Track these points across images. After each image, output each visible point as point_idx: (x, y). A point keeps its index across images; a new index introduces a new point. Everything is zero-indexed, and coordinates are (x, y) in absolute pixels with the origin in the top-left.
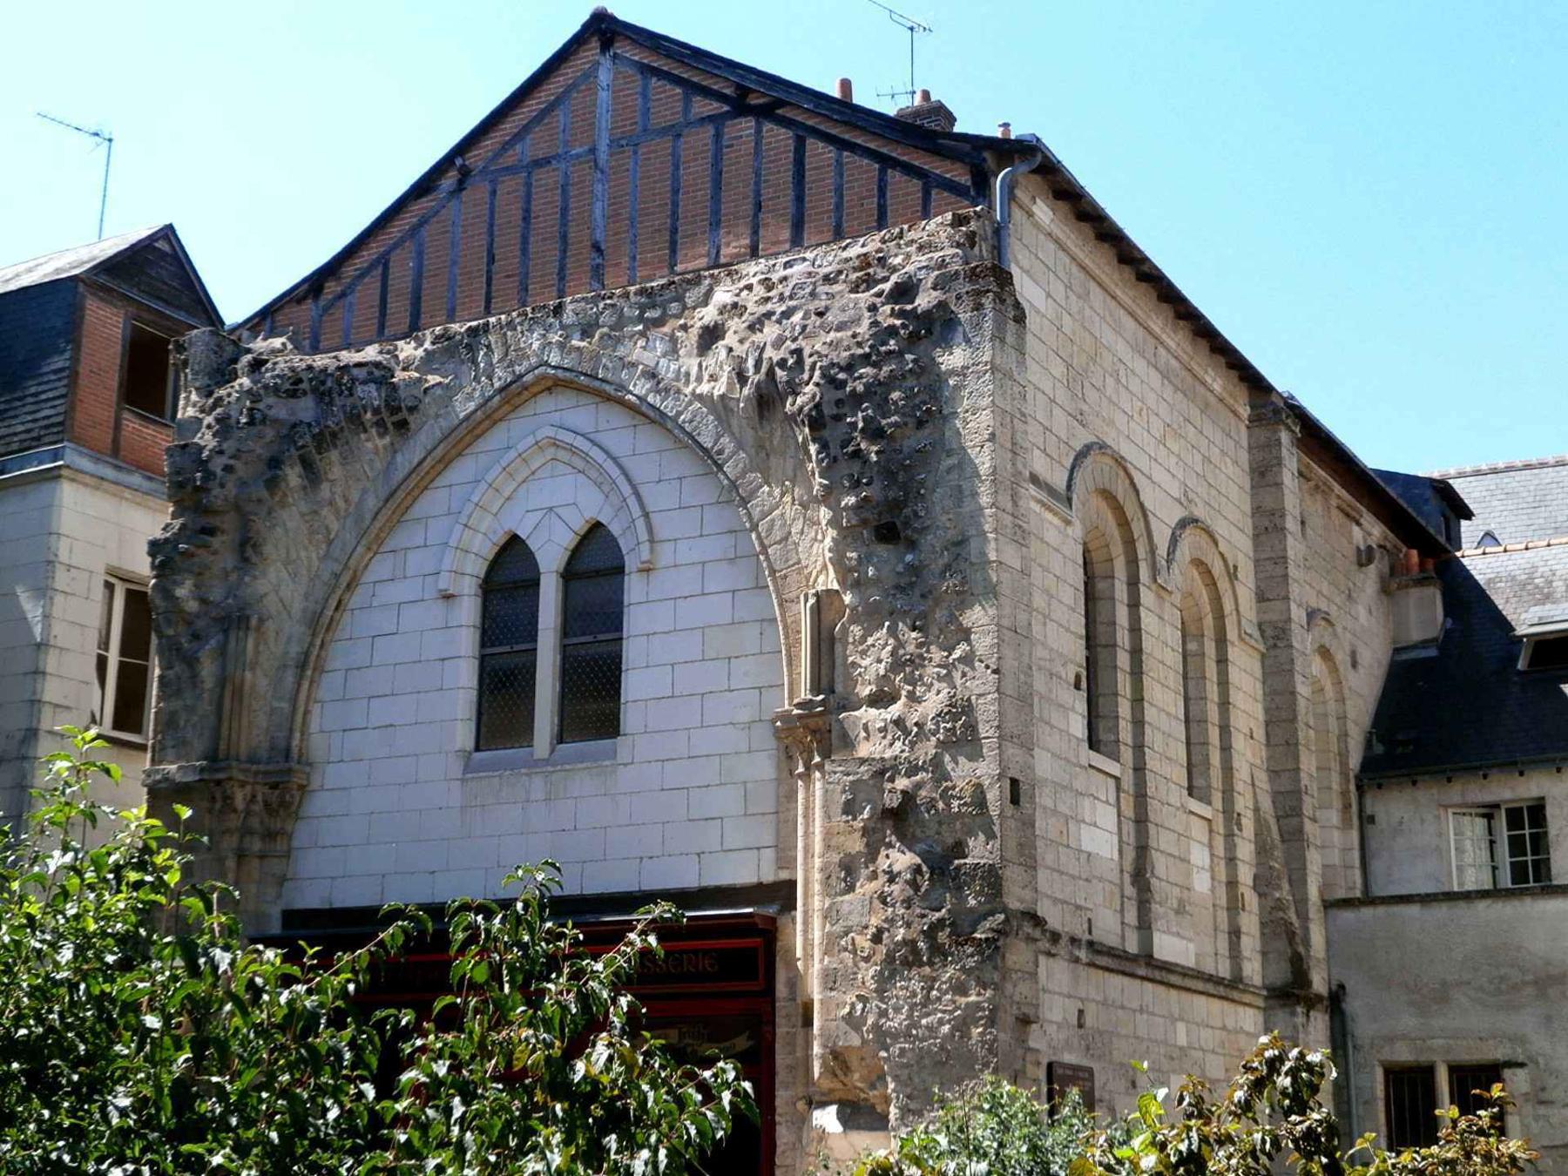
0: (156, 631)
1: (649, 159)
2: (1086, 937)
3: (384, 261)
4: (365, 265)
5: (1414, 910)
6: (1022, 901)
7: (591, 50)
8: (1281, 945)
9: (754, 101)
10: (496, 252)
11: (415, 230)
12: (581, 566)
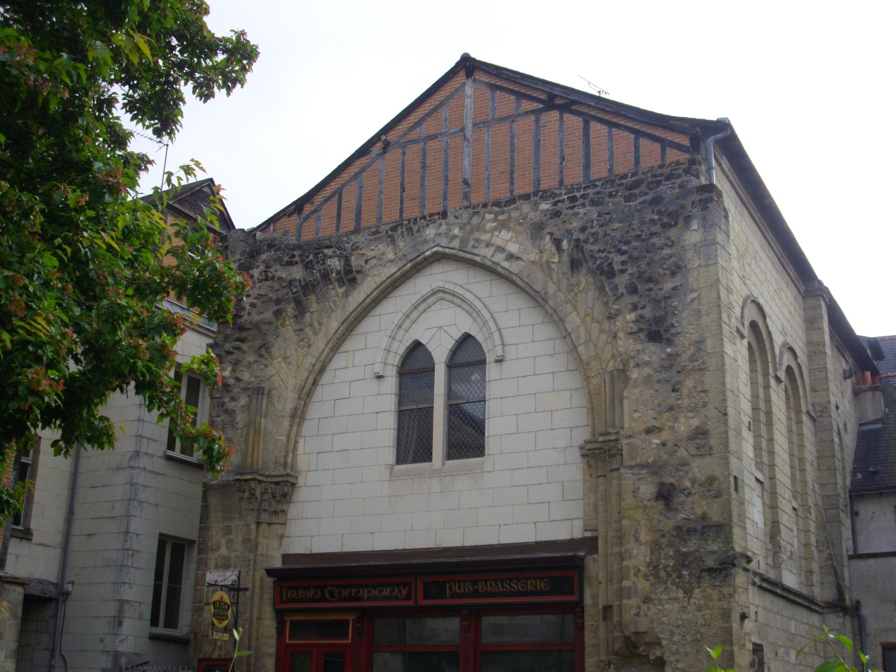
0: (688, 147)
1: (497, 134)
4: (328, 195)
6: (741, 547)
8: (831, 578)
9: (558, 102)
10: (405, 186)
11: (358, 174)
12: (461, 358)
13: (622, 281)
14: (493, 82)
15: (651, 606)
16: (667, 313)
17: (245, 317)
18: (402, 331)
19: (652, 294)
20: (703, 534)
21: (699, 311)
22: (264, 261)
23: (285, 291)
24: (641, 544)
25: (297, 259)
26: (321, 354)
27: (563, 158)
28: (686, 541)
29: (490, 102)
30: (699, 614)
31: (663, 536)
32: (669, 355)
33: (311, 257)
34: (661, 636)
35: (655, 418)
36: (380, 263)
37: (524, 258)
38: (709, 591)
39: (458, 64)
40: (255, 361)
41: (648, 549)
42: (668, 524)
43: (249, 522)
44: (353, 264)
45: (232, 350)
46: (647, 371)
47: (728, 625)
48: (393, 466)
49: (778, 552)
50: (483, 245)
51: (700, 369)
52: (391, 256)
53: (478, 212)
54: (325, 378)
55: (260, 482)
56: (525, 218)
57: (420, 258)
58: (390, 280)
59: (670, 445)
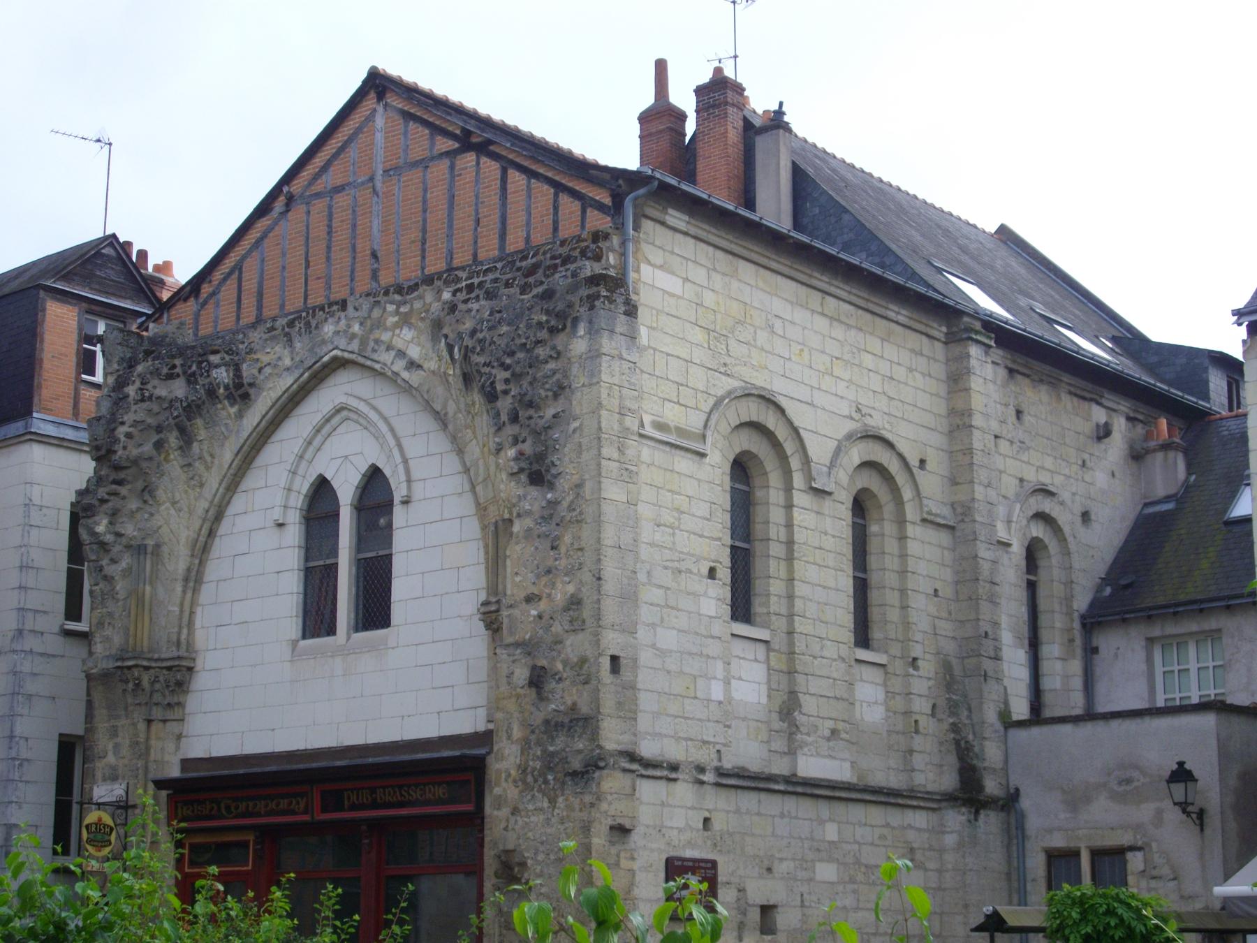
2: (715, 763)
3: (238, 267)
5: (1067, 728)
7: (369, 100)
9: (474, 140)
10: (310, 259)
13: (505, 404)
14: (406, 108)
15: (518, 818)
16: (547, 448)
17: (120, 453)
18: (304, 464)
19: (532, 422)
20: (569, 730)
21: (580, 445)
22: (139, 375)
23: (167, 414)
24: (512, 743)
25: (178, 370)
26: (215, 495)
27: (478, 222)
28: (553, 738)
29: (402, 137)
30: (562, 828)
31: (533, 732)
32: (549, 502)
33: (194, 368)
34: (526, 855)
35: (534, 583)
36: (276, 371)
37: (426, 366)
38: (571, 799)
39: (365, 82)
40: (139, 509)
41: (519, 747)
42: (538, 718)
43: (136, 720)
44: (245, 374)
45: (106, 497)
46: (528, 522)
47: (587, 840)
48: (298, 641)
49: (794, 733)
50: (383, 348)
51: (578, 521)
52: (287, 362)
53: (378, 302)
54: (224, 528)
55: (147, 668)
56: (427, 311)
57: (317, 365)
58: (286, 395)
59: (546, 617)
